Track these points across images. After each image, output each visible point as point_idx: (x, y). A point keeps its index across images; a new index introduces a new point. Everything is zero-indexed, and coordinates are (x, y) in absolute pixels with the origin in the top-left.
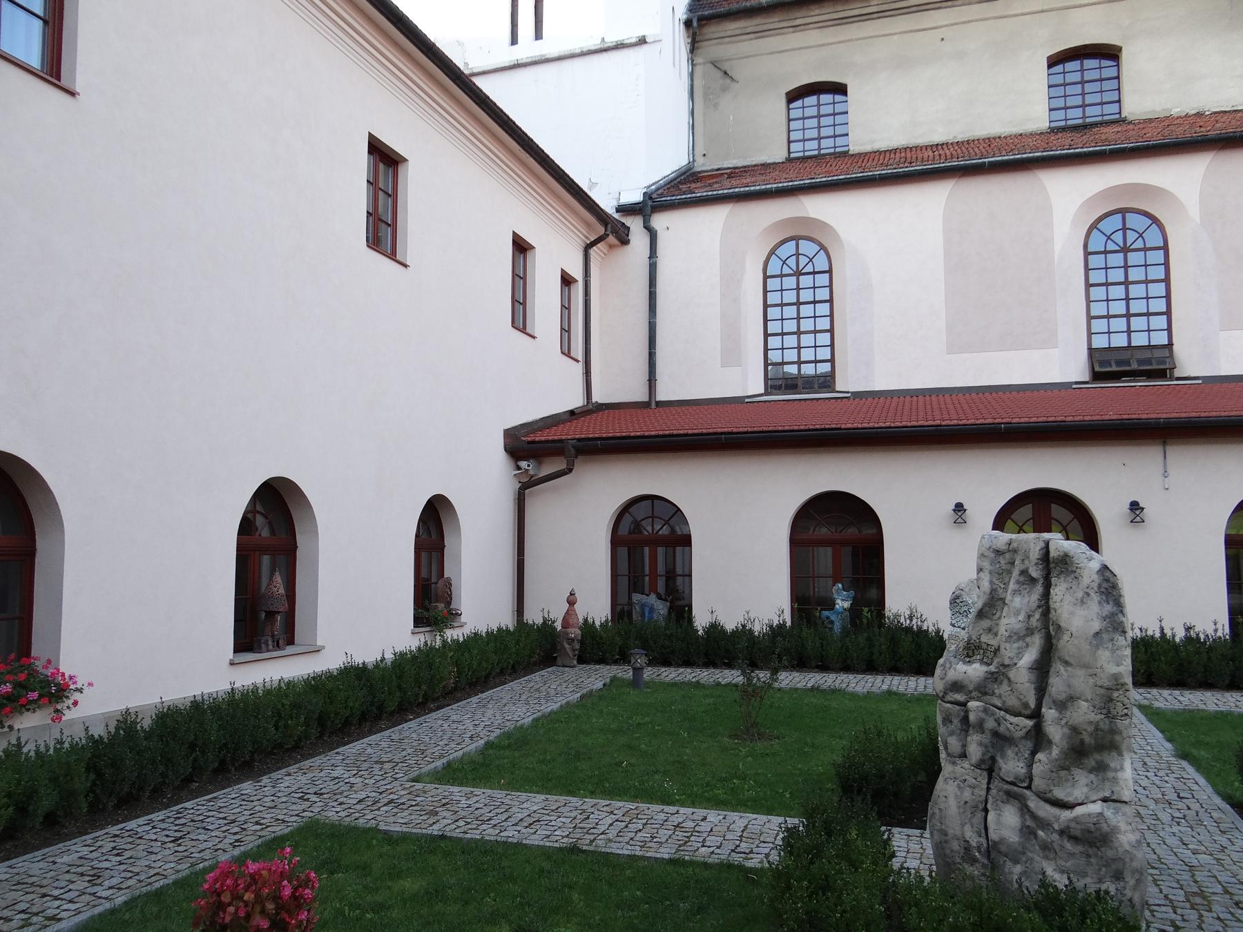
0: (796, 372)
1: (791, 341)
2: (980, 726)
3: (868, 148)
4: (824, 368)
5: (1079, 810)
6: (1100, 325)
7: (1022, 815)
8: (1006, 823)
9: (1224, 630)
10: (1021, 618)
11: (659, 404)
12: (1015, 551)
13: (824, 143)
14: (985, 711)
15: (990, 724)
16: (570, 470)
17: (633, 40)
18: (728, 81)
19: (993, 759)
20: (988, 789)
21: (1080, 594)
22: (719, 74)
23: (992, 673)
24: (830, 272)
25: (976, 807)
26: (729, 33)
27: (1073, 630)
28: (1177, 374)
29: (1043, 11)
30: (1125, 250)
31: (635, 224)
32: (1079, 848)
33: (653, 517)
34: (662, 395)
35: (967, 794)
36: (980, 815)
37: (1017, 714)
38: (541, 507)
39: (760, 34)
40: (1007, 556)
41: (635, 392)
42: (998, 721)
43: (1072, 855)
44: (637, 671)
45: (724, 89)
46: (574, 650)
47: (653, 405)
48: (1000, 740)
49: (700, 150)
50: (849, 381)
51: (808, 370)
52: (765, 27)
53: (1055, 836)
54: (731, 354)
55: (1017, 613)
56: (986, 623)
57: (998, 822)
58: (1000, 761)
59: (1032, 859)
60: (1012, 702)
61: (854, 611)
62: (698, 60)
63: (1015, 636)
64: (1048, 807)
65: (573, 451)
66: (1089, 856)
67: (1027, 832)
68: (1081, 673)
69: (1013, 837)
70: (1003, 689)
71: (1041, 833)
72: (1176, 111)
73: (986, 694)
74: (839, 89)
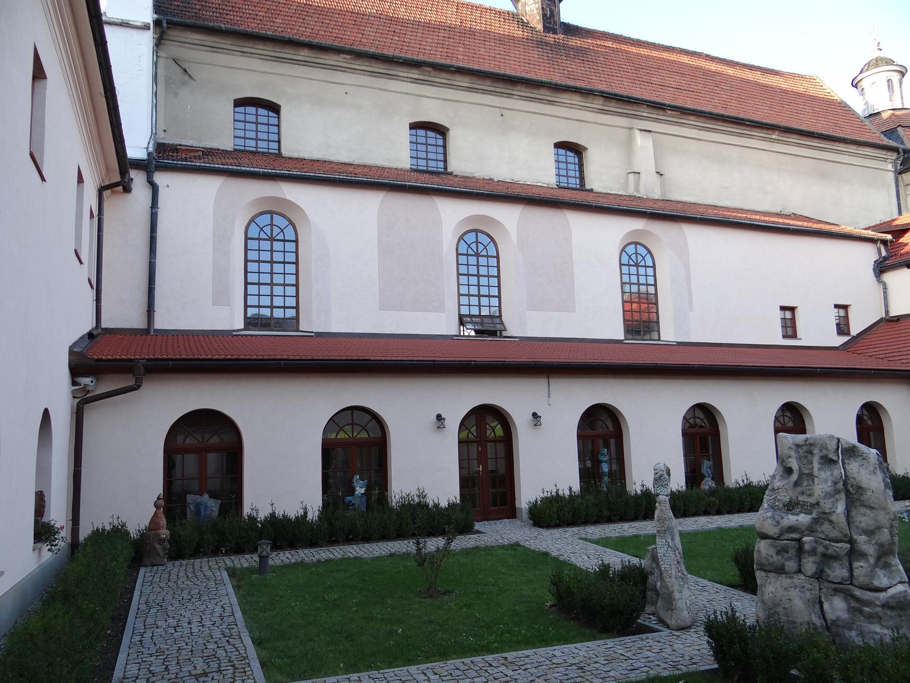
0: (269, 314)
1: (266, 290)
2: (813, 552)
3: (295, 155)
4: (291, 313)
5: (891, 591)
6: (464, 300)
7: (846, 601)
8: (837, 607)
9: (576, 488)
10: (829, 484)
11: (108, 331)
12: (812, 445)
13: (260, 144)
14: (816, 542)
15: (821, 549)
16: (139, 387)
17: (139, 24)
18: (187, 77)
19: (822, 571)
20: (820, 589)
21: (872, 468)
22: (178, 69)
23: (815, 519)
24: (296, 241)
25: (814, 602)
26: (190, 41)
27: (874, 489)
28: (504, 334)
29: (407, 94)
30: (272, 239)
31: (138, 178)
32: (894, 613)
33: (341, 429)
34: (160, 323)
35: (808, 595)
36: (818, 606)
37: (838, 541)
38: (98, 420)
39: (214, 49)
40: (804, 448)
41: (136, 321)
42: (826, 548)
43: (891, 618)
44: (263, 559)
45: (183, 83)
46: (164, 549)
47: (152, 333)
48: (827, 558)
49: (161, 126)
50: (311, 323)
51: (278, 313)
52: (220, 46)
53: (878, 609)
54: (220, 297)
55: (826, 481)
56: (799, 489)
57: (832, 608)
58: (828, 571)
59: (861, 626)
60: (835, 534)
61: (367, 494)
62: (161, 54)
63: (828, 495)
64: (870, 593)
65: (142, 370)
66: (901, 616)
67: (851, 610)
68: (882, 513)
69: (845, 616)
70: (826, 527)
71: (866, 609)
72: (477, 175)
73: (813, 531)
74: (275, 108)
